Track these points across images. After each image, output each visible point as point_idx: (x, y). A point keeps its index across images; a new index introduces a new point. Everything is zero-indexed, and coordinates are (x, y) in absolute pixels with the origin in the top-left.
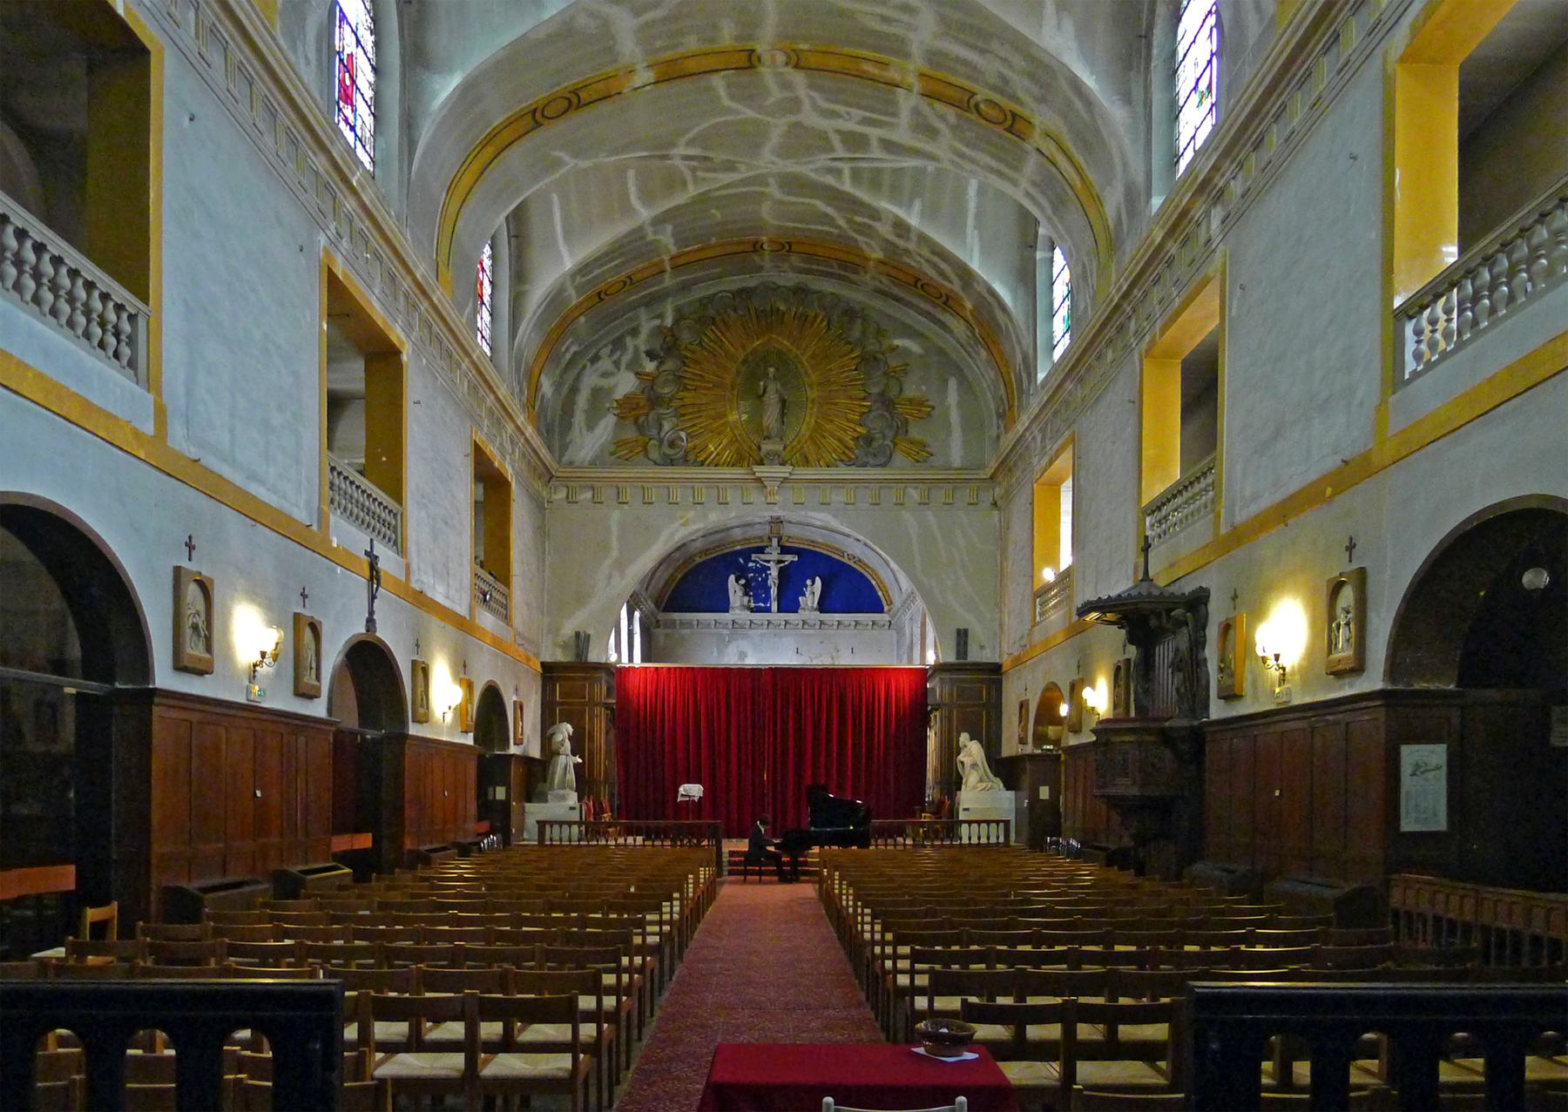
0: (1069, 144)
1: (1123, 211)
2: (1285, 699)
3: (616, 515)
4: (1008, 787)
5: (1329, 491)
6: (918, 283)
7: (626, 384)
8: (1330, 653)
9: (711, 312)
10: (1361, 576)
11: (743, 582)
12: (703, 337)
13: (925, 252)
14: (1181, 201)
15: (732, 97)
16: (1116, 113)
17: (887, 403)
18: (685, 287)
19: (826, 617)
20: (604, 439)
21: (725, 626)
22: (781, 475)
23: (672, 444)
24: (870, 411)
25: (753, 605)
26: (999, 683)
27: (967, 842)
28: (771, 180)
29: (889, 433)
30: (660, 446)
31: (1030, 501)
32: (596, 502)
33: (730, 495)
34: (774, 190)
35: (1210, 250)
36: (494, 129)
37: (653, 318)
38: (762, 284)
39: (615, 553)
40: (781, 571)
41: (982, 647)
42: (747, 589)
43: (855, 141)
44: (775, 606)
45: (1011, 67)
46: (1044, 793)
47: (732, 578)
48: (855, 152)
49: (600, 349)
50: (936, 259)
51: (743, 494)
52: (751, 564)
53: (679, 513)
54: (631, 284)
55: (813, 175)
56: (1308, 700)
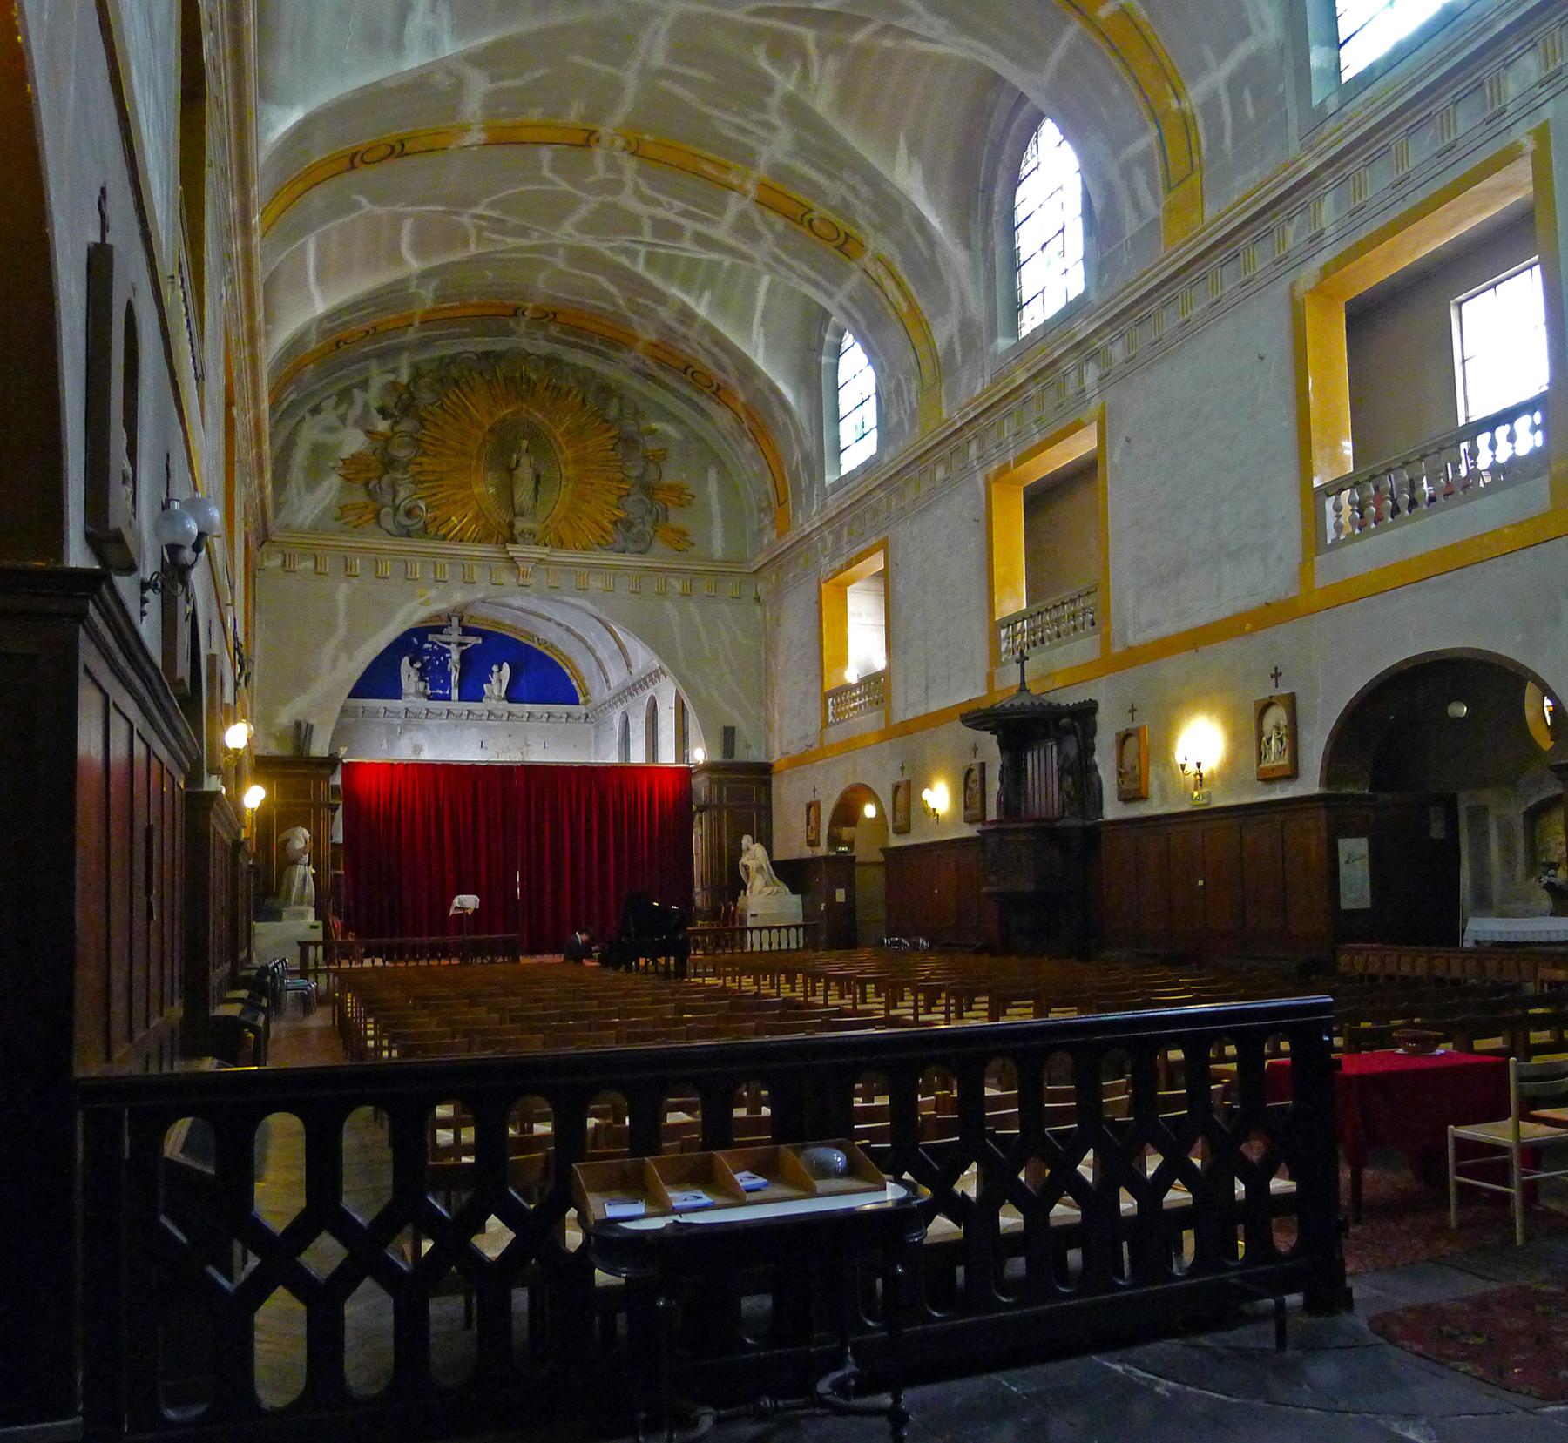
0: (898, 267)
1: (956, 340)
2: (1205, 801)
3: (343, 591)
4: (794, 891)
5: (1248, 627)
6: (689, 371)
7: (354, 442)
8: (1260, 762)
9: (455, 373)
10: (1291, 703)
11: (418, 665)
12: (445, 399)
13: (707, 342)
14: (1052, 352)
15: (553, 169)
16: (955, 254)
17: (649, 489)
18: (425, 344)
19: (516, 707)
20: (327, 501)
21: (397, 715)
22: (536, 556)
23: (409, 513)
24: (628, 494)
25: (429, 692)
26: (768, 784)
27: (759, 949)
28: (561, 251)
29: (649, 519)
30: (395, 514)
31: (815, 599)
32: (318, 572)
33: (478, 573)
34: (560, 262)
35: (1083, 400)
36: (309, 168)
37: (384, 372)
38: (511, 348)
39: (342, 632)
40: (463, 655)
41: (749, 746)
42: (422, 676)
43: (667, 230)
44: (455, 694)
45: (857, 196)
46: (840, 896)
47: (406, 660)
48: (662, 239)
49: (324, 399)
50: (715, 350)
51: (491, 575)
52: (427, 646)
53: (419, 591)
54: (375, 334)
55: (608, 253)
56: (1232, 802)
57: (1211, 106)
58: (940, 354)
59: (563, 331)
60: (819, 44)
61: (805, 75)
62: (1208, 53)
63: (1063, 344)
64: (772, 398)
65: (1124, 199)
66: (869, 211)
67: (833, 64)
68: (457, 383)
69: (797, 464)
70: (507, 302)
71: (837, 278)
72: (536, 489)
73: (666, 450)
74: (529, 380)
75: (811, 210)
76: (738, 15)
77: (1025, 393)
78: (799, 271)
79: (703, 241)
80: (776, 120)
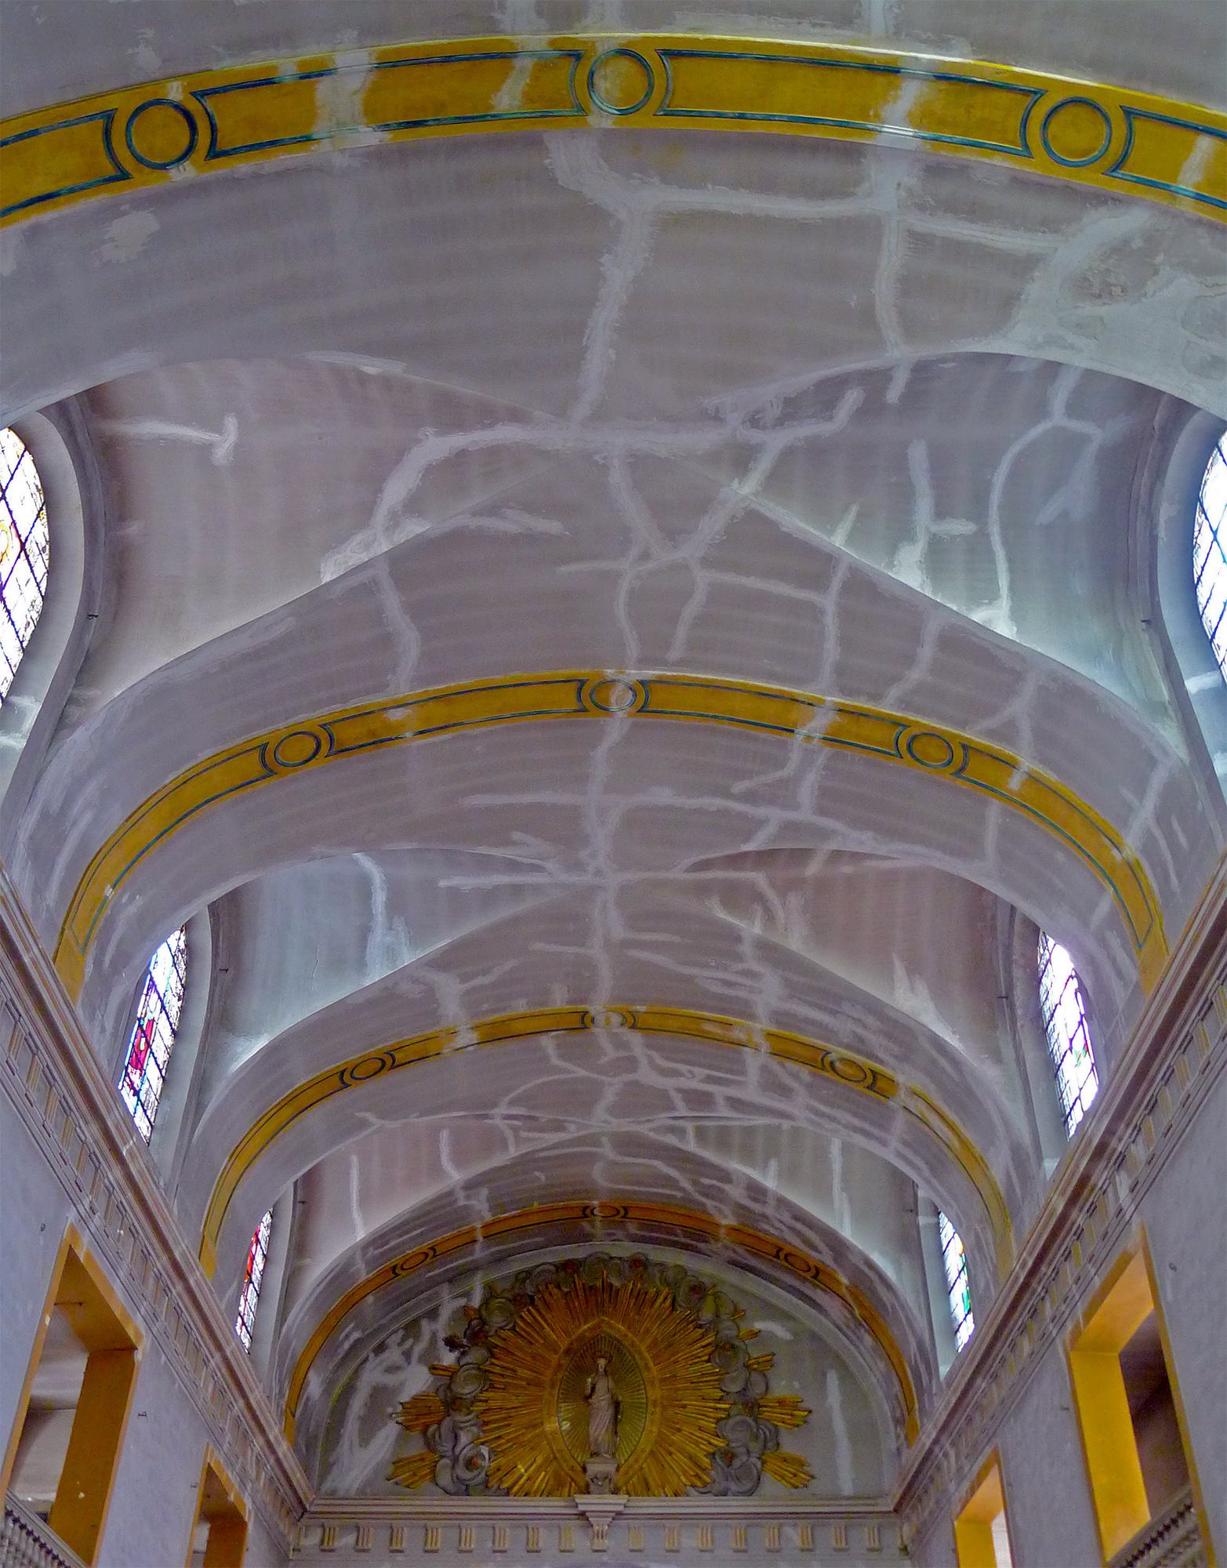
6: (782, 1256)
7: (417, 1381)
9: (530, 1289)
13: (786, 1217)
14: (1077, 1166)
15: (562, 1057)
17: (752, 1407)
18: (499, 1259)
23: (470, 1464)
29: (756, 1447)
30: (453, 1467)
34: (608, 1151)
43: (700, 1100)
45: (865, 1026)
50: (799, 1226)
57: (1148, 847)
58: (1003, 1192)
59: (642, 1227)
60: (772, 884)
61: (770, 918)
62: (1127, 794)
63: (1084, 1154)
64: (871, 1274)
65: (1108, 969)
66: (885, 1042)
67: (795, 900)
68: (532, 1298)
69: (915, 1354)
70: (573, 1203)
71: (884, 1122)
72: (615, 1421)
73: (774, 1354)
74: (611, 1286)
75: (828, 1053)
76: (678, 874)
77: (1073, 1224)
78: (844, 1122)
79: (735, 1103)
80: (756, 967)
